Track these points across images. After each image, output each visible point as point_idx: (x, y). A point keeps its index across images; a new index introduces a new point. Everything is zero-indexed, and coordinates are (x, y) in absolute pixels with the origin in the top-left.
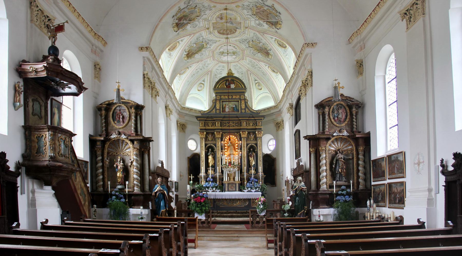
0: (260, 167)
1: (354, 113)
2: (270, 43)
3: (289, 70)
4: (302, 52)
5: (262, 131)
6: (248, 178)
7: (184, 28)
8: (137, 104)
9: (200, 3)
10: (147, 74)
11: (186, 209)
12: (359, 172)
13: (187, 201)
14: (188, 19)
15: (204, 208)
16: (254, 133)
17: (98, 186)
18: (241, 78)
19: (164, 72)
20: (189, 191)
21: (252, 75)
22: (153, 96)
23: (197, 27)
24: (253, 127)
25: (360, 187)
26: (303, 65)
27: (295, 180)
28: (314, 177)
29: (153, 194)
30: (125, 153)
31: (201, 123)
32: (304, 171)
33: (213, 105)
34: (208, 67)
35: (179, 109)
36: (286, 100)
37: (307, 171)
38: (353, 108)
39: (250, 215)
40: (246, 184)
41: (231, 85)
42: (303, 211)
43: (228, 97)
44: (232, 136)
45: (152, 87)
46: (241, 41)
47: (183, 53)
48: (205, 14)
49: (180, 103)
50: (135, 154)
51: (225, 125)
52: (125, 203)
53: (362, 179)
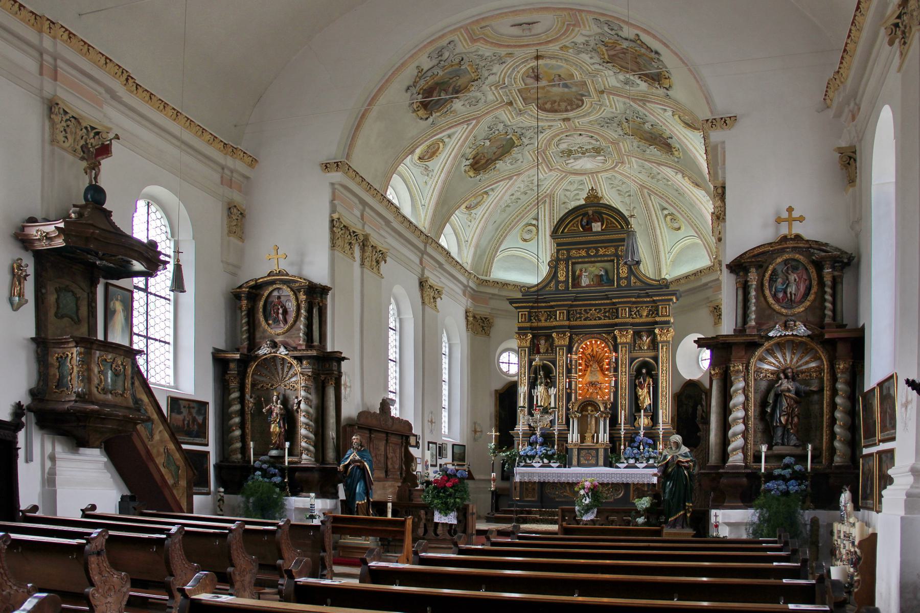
0: (623, 412)
1: (828, 280)
5: (670, 327)
7: (446, 110)
8: (310, 282)
9: (472, 53)
10: (339, 219)
12: (835, 423)
14: (451, 89)
16: (651, 333)
17: (232, 451)
21: (652, 197)
23: (480, 104)
24: (650, 319)
25: (835, 460)
28: (716, 435)
30: (289, 384)
38: (824, 269)
41: (593, 224)
43: (587, 252)
48: (491, 72)
50: (303, 387)
51: (578, 316)
52: (282, 486)
53: (840, 440)
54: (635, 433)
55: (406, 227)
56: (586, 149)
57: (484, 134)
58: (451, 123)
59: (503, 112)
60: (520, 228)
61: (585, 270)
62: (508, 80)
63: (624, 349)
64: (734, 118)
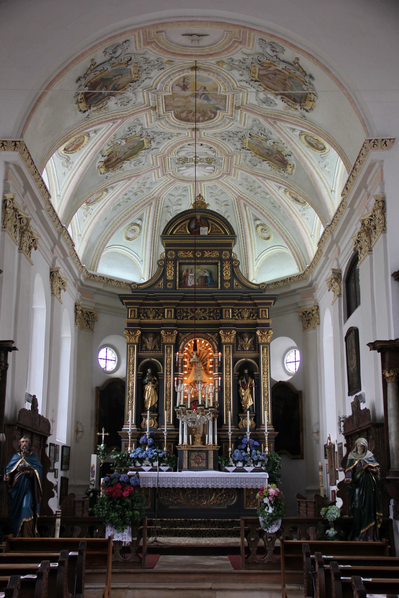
0: (266, 412)
2: (289, 139)
3: (330, 197)
4: (360, 159)
5: (271, 329)
6: (237, 439)
7: (101, 106)
9: (140, 54)
10: (12, 199)
11: (86, 515)
13: (88, 494)
14: (111, 86)
15: (129, 513)
16: (252, 334)
18: (225, 213)
19: (52, 196)
20: (95, 469)
21: (247, 208)
22: (24, 248)
23: (129, 105)
24: (250, 321)
26: (363, 185)
27: (350, 445)
29: (6, 477)
31: (131, 311)
32: (370, 424)
33: (160, 270)
34: (152, 190)
35: (82, 278)
36: (325, 262)
37: (378, 424)
39: (243, 527)
40: (232, 452)
41: (201, 228)
42: (373, 523)
43: (194, 254)
44: (200, 341)
45: (21, 228)
46: (226, 137)
47: (98, 157)
48: (149, 76)
49: (84, 265)
51: (185, 314)
54: (240, 435)
55: (50, 215)
56: (201, 159)
57: (122, 134)
58: (101, 119)
59: (145, 115)
60: (126, 228)
61: (191, 270)
62: (161, 86)
63: (228, 349)
64: (392, 140)
